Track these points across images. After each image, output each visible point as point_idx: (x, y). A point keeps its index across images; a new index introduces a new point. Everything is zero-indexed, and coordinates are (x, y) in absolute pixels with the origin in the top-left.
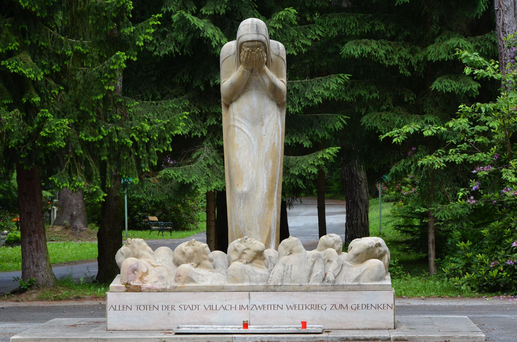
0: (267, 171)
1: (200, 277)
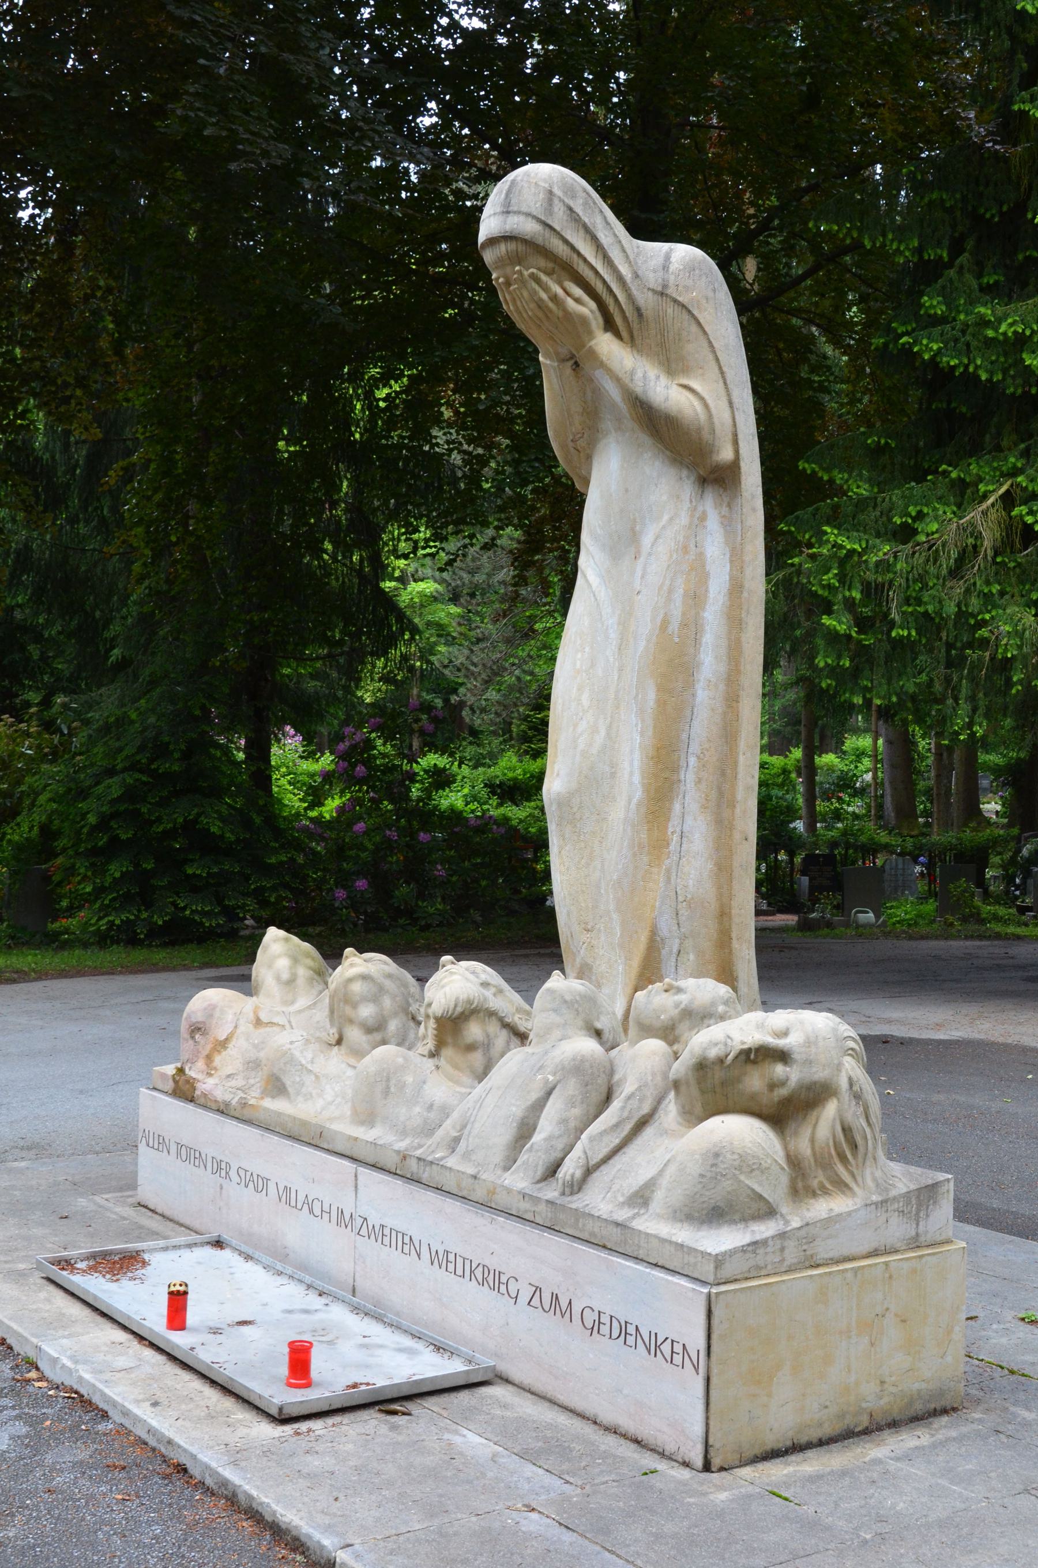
0: (643, 721)
1: (309, 1080)
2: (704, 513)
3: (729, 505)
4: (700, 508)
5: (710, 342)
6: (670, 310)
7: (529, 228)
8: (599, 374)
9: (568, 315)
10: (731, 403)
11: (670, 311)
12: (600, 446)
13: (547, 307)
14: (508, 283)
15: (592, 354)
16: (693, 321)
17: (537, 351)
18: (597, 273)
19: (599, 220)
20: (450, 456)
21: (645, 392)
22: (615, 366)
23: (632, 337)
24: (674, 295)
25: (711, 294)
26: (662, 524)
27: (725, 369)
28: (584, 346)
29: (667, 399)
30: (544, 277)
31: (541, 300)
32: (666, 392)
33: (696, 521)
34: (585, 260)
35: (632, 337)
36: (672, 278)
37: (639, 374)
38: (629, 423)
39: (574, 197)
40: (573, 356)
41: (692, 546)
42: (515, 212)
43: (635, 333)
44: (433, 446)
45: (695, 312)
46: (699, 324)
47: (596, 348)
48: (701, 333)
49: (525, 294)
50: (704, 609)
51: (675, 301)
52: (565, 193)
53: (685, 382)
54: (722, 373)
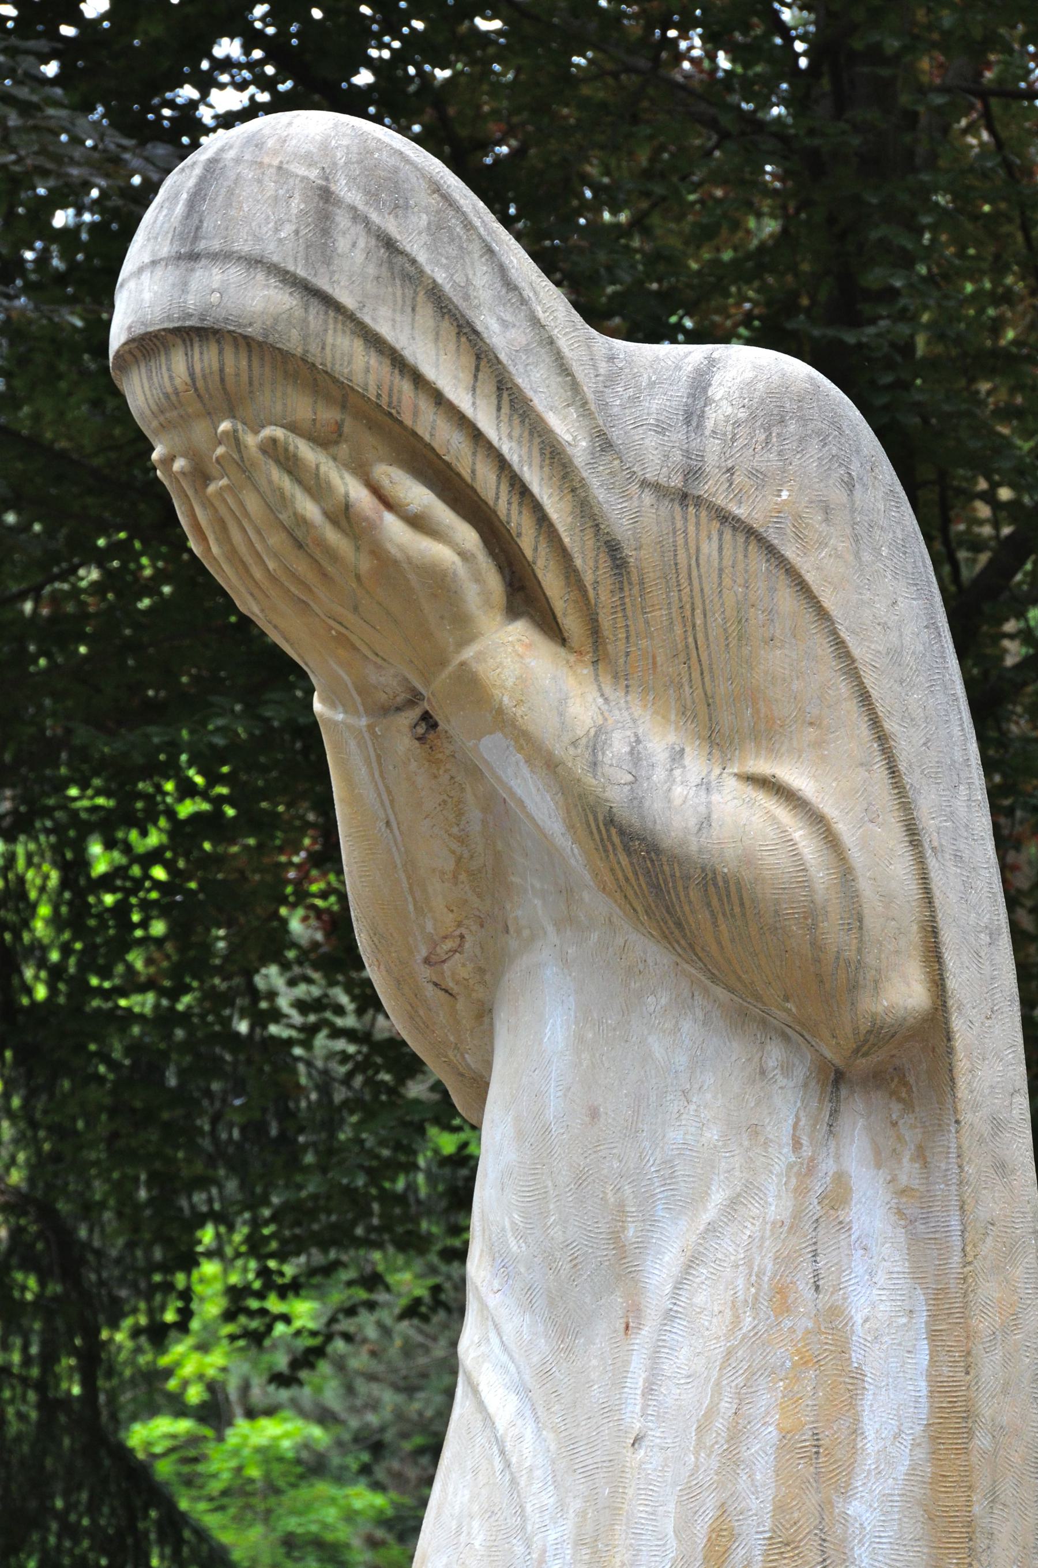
2: (841, 1179)
3: (921, 1155)
4: (828, 1166)
5: (839, 644)
6: (711, 546)
7: (260, 301)
8: (491, 748)
9: (388, 567)
10: (913, 832)
11: (709, 548)
12: (514, 976)
13: (321, 543)
14: (201, 475)
15: (471, 687)
16: (783, 582)
17: (310, 691)
18: (476, 436)
19: (481, 279)
20: (307, 1044)
21: (636, 801)
22: (540, 720)
23: (595, 631)
24: (720, 501)
25: (838, 496)
27: (890, 725)
29: (706, 822)
30: (307, 452)
31: (302, 521)
32: (703, 801)
33: (815, 1208)
34: (438, 398)
35: (595, 631)
36: (713, 448)
37: (618, 745)
38: (596, 903)
39: (400, 207)
40: (415, 698)
41: (804, 1287)
42: (215, 257)
43: (605, 621)
44: (261, 1019)
45: (790, 552)
46: (802, 587)
47: (480, 668)
48: (809, 616)
49: (252, 503)
50: (846, 1491)
51: (724, 517)
52: (373, 196)
53: (763, 767)
54: (882, 738)
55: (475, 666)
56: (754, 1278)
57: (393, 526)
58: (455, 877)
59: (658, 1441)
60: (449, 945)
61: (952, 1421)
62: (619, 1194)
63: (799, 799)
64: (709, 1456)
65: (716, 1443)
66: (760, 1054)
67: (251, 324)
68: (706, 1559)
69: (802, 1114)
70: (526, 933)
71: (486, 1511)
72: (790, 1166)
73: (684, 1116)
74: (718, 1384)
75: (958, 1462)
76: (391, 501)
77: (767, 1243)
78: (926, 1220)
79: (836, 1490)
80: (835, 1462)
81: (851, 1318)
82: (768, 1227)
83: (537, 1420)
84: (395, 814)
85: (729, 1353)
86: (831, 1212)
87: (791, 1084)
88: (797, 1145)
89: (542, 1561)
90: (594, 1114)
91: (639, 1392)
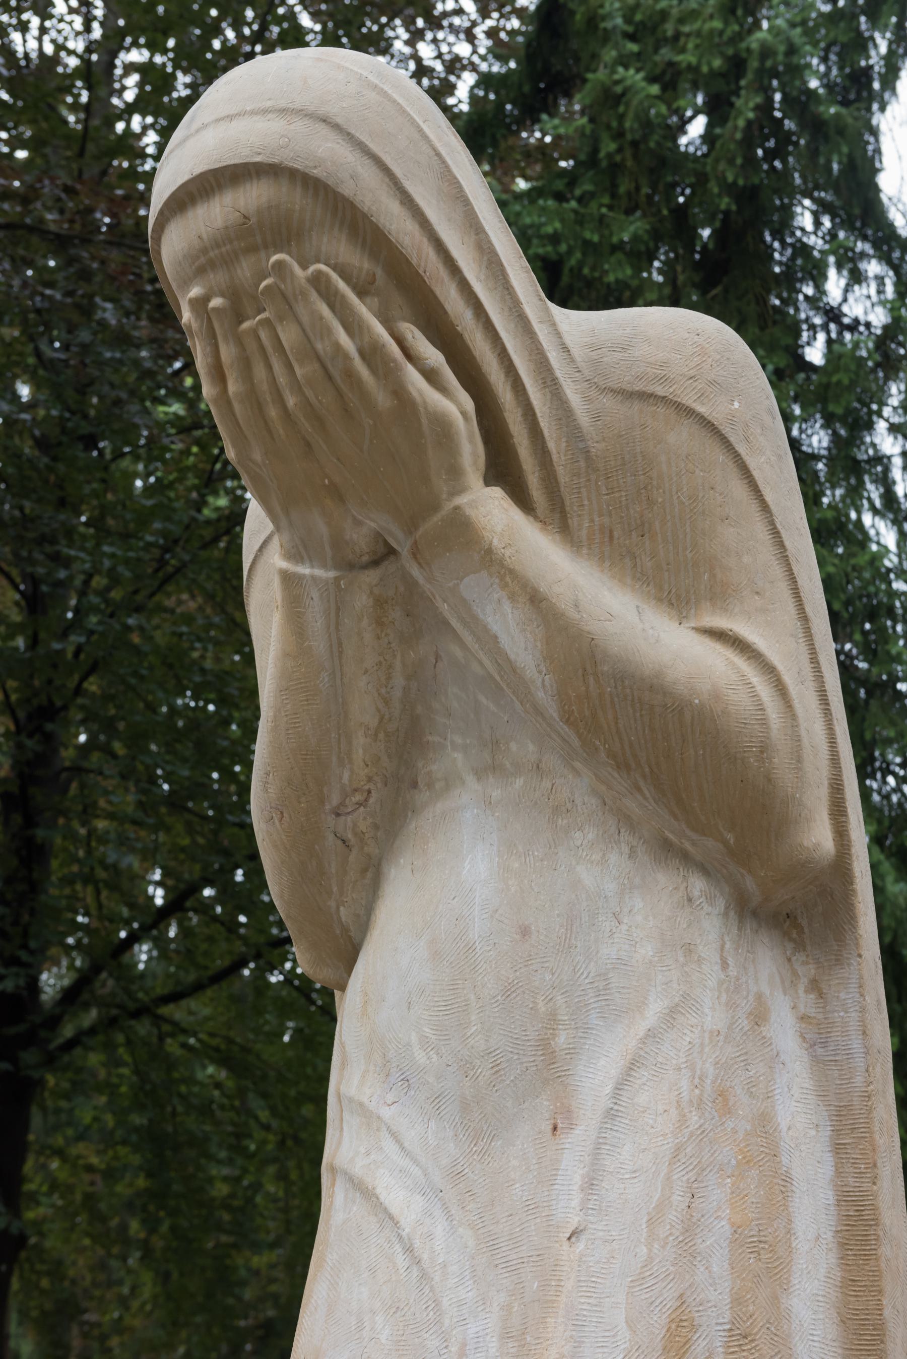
3: (815, 986)
13: (350, 374)
26: (641, 1027)
28: (435, 507)
32: (667, 644)
33: (745, 1024)
45: (741, 449)
47: (471, 512)
55: (469, 512)
56: (697, 1081)
57: (414, 377)
58: (376, 735)
59: (601, 1234)
60: (358, 797)
61: (857, 1232)
62: (551, 1004)
63: (754, 651)
64: (663, 1247)
65: (671, 1234)
66: (685, 884)
67: (315, 167)
68: (665, 1350)
69: (726, 938)
70: (439, 785)
71: (390, 1307)
72: (721, 983)
73: (615, 936)
74: (668, 1178)
75: (867, 1267)
76: (412, 352)
77: (707, 1050)
78: (824, 1045)
79: (781, 1287)
80: (778, 1258)
81: (778, 1125)
82: (707, 1035)
83: (449, 1217)
84: (341, 666)
85: (678, 1149)
86: (756, 1027)
87: (716, 912)
88: (725, 965)
89: (462, 1353)
90: (525, 932)
91: (576, 1187)
